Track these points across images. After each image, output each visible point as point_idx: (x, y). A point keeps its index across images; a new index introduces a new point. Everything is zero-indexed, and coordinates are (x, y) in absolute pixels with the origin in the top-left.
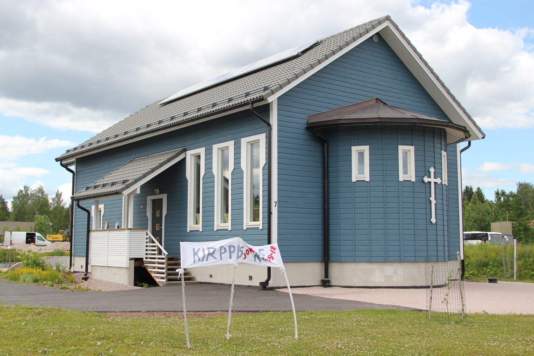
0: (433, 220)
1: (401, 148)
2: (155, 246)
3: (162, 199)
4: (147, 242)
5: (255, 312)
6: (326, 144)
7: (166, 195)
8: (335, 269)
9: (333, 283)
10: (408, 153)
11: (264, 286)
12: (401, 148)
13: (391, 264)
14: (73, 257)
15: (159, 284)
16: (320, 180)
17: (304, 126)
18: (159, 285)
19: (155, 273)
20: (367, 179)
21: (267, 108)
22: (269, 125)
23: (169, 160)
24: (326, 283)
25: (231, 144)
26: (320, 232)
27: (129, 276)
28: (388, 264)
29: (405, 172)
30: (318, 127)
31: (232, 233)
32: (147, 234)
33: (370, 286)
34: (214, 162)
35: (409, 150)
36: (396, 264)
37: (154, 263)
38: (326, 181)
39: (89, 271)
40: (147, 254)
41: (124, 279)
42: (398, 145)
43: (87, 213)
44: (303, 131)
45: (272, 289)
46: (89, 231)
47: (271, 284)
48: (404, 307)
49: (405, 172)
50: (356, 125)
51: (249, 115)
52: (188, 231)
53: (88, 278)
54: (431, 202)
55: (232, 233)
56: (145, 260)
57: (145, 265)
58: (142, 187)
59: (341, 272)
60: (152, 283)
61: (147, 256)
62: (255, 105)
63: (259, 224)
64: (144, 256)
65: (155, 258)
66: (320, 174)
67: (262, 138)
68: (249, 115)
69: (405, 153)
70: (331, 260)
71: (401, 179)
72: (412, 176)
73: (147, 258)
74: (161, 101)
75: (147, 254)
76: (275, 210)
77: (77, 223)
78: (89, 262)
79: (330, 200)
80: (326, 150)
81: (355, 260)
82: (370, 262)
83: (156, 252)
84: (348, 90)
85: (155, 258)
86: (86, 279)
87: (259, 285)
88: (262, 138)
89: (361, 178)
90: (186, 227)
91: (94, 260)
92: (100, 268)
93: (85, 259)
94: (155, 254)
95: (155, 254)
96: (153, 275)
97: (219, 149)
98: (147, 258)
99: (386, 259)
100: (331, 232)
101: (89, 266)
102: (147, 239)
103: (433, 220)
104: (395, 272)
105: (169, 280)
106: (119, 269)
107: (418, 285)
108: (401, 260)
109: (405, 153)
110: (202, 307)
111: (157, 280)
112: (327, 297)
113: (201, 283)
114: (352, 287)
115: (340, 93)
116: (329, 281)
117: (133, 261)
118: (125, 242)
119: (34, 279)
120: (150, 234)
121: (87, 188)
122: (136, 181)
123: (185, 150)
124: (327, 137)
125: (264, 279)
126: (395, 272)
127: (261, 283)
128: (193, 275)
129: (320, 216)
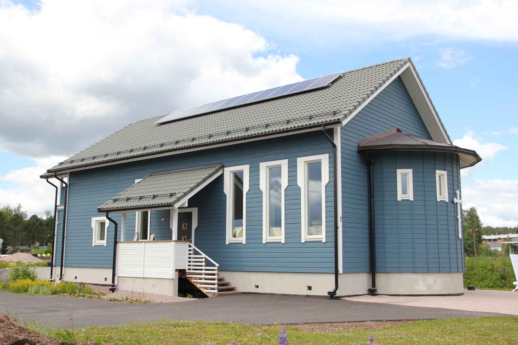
0: (460, 236)
1: (399, 172)
2: (202, 258)
3: (191, 213)
4: (190, 254)
5: (399, 321)
6: (371, 166)
7: (197, 208)
8: (381, 279)
9: (379, 291)
10: (442, 178)
11: (332, 295)
12: (399, 172)
13: (432, 274)
14: (63, 268)
15: (207, 295)
16: (366, 198)
17: (356, 149)
18: (207, 296)
19: (201, 283)
20: (412, 199)
21: (331, 132)
22: (334, 146)
23: (210, 176)
24: (372, 292)
25: (284, 164)
26: (367, 245)
27: (174, 287)
28: (429, 274)
29: (404, 192)
30: (369, 150)
31: (285, 246)
32: (190, 246)
33: (415, 294)
34: (266, 179)
35: (443, 175)
36: (435, 274)
37: (201, 274)
38: (372, 199)
39: (116, 283)
40: (189, 265)
41: (169, 290)
42: (435, 169)
43: (114, 225)
44: (355, 154)
45: (338, 298)
46: (116, 243)
47: (338, 293)
48: (504, 314)
49: (404, 192)
50: (388, 150)
51: (315, 137)
52: (227, 243)
53: (115, 289)
54: (458, 220)
55: (285, 246)
56: (187, 271)
57: (187, 276)
58: (190, 200)
59: (383, 281)
60: (199, 294)
61: (190, 267)
62: (327, 127)
63: (322, 237)
64: (187, 268)
65: (201, 270)
66: (366, 193)
67: (324, 159)
68: (315, 137)
69: (404, 176)
70: (377, 271)
71: (399, 199)
72: (410, 196)
73: (189, 269)
74: (162, 117)
75: (189, 265)
76: (340, 224)
77: (69, 235)
78: (116, 273)
79: (376, 217)
80: (371, 171)
81: (400, 270)
82: (414, 272)
83: (204, 264)
84: (381, 120)
85: (201, 270)
86: (113, 290)
87: (327, 294)
88: (324, 159)
89: (405, 197)
90: (225, 239)
91: (120, 271)
92: (131, 280)
93: (111, 271)
94: (202, 266)
95: (202, 266)
96: (199, 286)
97: (267, 167)
98: (189, 269)
99: (428, 270)
100: (377, 246)
101: (116, 277)
102: (190, 250)
103: (460, 236)
104: (435, 282)
105: (219, 291)
106: (160, 280)
107: (452, 293)
108: (439, 271)
109: (404, 176)
110: (324, 317)
111: (205, 291)
112: (399, 304)
113: (244, 293)
114: (387, 295)
115: (376, 122)
116: (376, 290)
117: (177, 272)
118: (172, 254)
119: (54, 290)
120: (192, 245)
121: (115, 200)
122: (185, 194)
123: (223, 167)
124: (374, 161)
125: (332, 289)
126: (435, 282)
127: (329, 293)
128: (233, 285)
129: (367, 231)
